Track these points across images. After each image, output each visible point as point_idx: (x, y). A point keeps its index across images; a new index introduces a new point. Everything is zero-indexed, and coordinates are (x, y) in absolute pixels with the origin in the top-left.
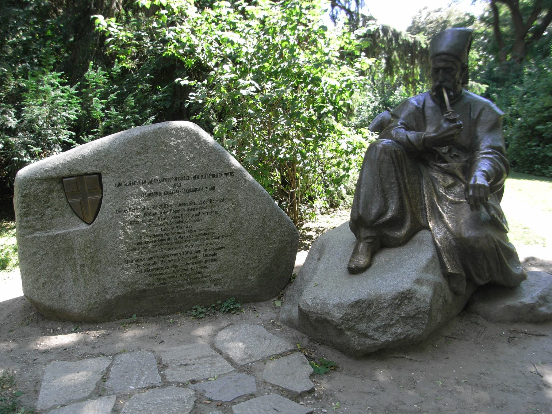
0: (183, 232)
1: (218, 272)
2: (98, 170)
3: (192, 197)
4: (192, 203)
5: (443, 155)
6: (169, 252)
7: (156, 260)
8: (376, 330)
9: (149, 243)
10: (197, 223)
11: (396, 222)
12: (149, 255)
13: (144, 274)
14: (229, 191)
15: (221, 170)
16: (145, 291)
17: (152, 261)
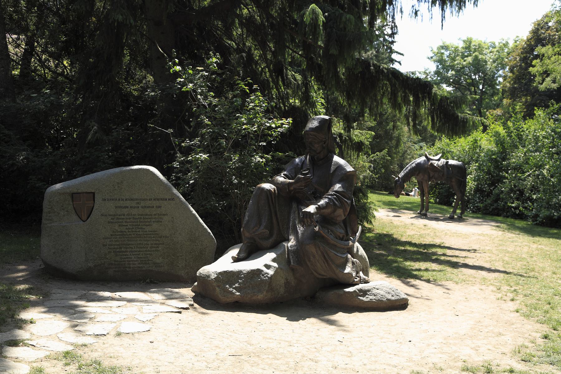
0: (139, 231)
2: (93, 191)
3: (147, 211)
6: (129, 243)
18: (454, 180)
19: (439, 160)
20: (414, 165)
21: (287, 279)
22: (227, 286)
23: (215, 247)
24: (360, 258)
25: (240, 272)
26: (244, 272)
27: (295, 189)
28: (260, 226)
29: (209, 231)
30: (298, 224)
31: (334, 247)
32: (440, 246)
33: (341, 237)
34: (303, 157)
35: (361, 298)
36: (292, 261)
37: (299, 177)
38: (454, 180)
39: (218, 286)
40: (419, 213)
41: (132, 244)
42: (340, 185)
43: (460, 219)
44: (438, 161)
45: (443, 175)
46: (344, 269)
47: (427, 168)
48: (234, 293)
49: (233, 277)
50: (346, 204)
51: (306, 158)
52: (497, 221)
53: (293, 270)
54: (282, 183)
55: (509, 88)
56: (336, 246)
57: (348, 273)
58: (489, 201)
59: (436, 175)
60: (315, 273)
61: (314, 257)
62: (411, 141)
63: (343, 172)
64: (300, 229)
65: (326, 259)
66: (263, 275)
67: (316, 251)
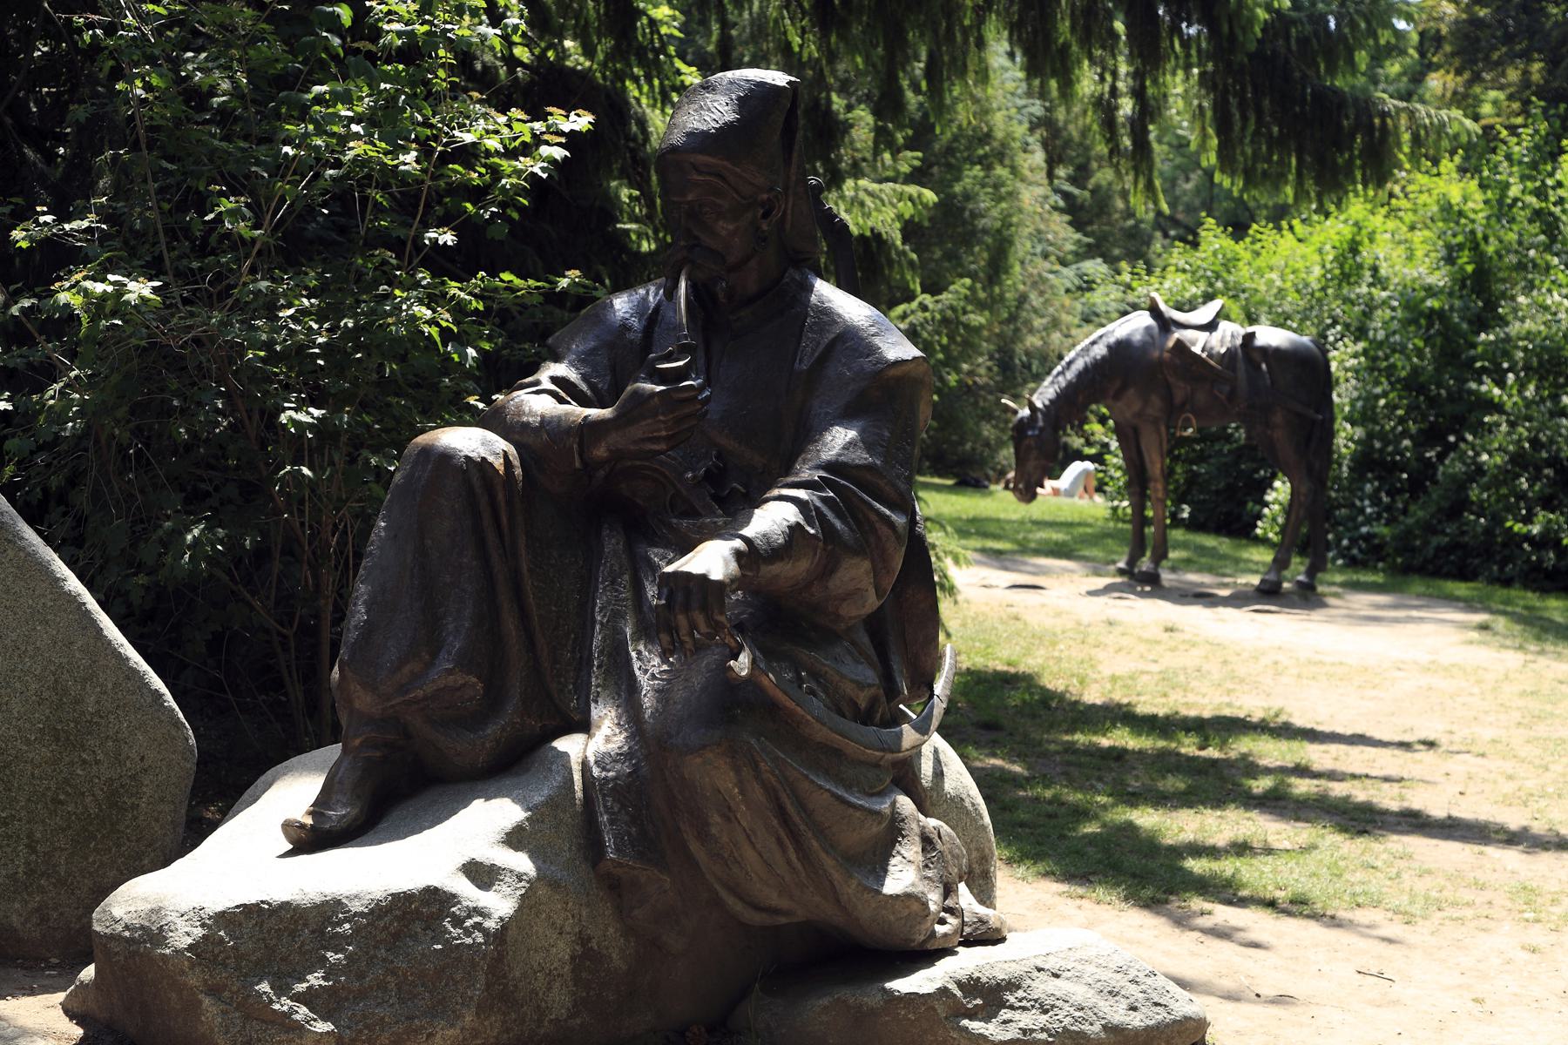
18: (1278, 418)
19: (1211, 327)
20: (1100, 351)
21: (583, 939)
22: (265, 987)
23: (191, 766)
24: (953, 809)
25: (330, 909)
26: (356, 907)
27: (617, 455)
28: (434, 655)
29: (157, 683)
30: (636, 640)
31: (830, 759)
32: (1287, 731)
33: (863, 705)
34: (651, 294)
35: (976, 1026)
36: (609, 841)
37: (637, 394)
38: (1278, 418)
39: (214, 991)
40: (1121, 572)
42: (852, 434)
43: (1307, 597)
44: (1211, 335)
45: (1232, 396)
46: (881, 871)
47: (1161, 362)
48: (299, 1028)
49: (293, 934)
50: (884, 530)
51: (671, 293)
52: (1469, 605)
53: (614, 886)
54: (547, 425)
55: (1457, 22)
56: (838, 753)
57: (908, 896)
58: (1419, 513)
59: (1201, 398)
60: (730, 901)
61: (728, 814)
62: (1046, 256)
63: (867, 363)
64: (649, 667)
65: (792, 822)
66: (458, 922)
67: (740, 784)
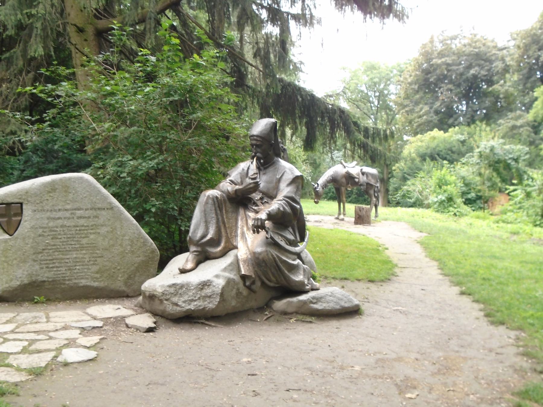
0: (75, 245)
1: (97, 273)
2: (21, 201)
3: (82, 222)
4: (83, 226)
5: (256, 201)
6: (64, 257)
7: (55, 261)
8: (184, 302)
9: (50, 249)
10: (85, 239)
11: (214, 242)
12: (50, 258)
13: (45, 270)
14: (109, 220)
15: (105, 205)
16: (44, 281)
17: (51, 262)
26: (194, 284)
41: (68, 259)
